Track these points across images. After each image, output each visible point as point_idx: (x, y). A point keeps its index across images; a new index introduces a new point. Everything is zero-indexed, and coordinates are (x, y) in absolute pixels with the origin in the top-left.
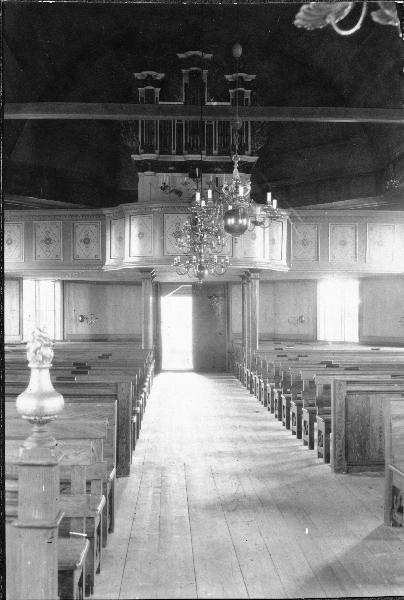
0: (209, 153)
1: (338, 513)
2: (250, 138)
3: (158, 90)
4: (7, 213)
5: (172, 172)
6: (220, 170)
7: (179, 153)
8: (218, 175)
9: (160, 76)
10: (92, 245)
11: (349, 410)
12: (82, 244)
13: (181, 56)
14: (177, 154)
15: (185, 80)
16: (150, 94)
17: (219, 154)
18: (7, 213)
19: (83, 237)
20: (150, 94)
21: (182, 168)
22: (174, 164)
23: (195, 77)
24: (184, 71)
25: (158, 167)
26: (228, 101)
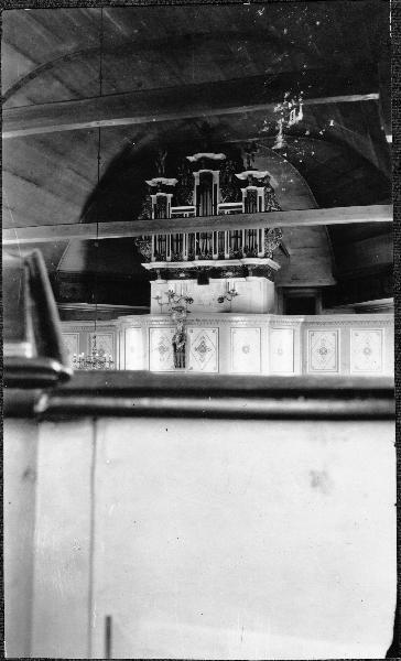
0: (221, 258)
1: (337, 578)
2: (263, 238)
3: (170, 196)
4: (392, 385)
5: (182, 278)
6: (231, 274)
7: (191, 259)
8: (229, 280)
9: (172, 182)
10: (208, 355)
11: (86, 609)
12: (196, 353)
13: (191, 159)
14: (189, 260)
15: (197, 182)
16: (162, 200)
17: (231, 258)
18: (392, 385)
19: (197, 344)
20: (162, 200)
21: (193, 274)
22: (181, 270)
23: (207, 178)
24: (195, 173)
25: (167, 275)
26: (240, 200)
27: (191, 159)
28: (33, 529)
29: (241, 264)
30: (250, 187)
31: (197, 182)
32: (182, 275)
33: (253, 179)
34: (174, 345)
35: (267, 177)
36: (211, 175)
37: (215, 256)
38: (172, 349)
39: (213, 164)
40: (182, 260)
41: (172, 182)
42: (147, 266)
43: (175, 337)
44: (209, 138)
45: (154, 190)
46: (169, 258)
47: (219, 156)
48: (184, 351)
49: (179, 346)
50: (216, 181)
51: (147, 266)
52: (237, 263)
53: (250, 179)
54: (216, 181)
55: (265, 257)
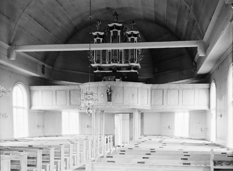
0: (121, 63)
7: (110, 63)
9: (102, 34)
13: (110, 25)
15: (112, 34)
24: (111, 31)
27: (110, 25)
28: (42, 71)
29: (128, 65)
30: (98, 38)
31: (112, 34)
32: (106, 69)
33: (134, 34)
34: (108, 93)
35: (138, 34)
36: (117, 32)
37: (119, 62)
38: (107, 94)
39: (118, 28)
40: (106, 63)
41: (102, 34)
42: (93, 65)
43: (108, 90)
44: (115, 14)
45: (96, 37)
46: (101, 63)
47: (121, 25)
48: (111, 95)
49: (110, 93)
50: (119, 34)
51: (93, 65)
52: (127, 65)
53: (98, 35)
54: (119, 34)
55: (137, 63)
